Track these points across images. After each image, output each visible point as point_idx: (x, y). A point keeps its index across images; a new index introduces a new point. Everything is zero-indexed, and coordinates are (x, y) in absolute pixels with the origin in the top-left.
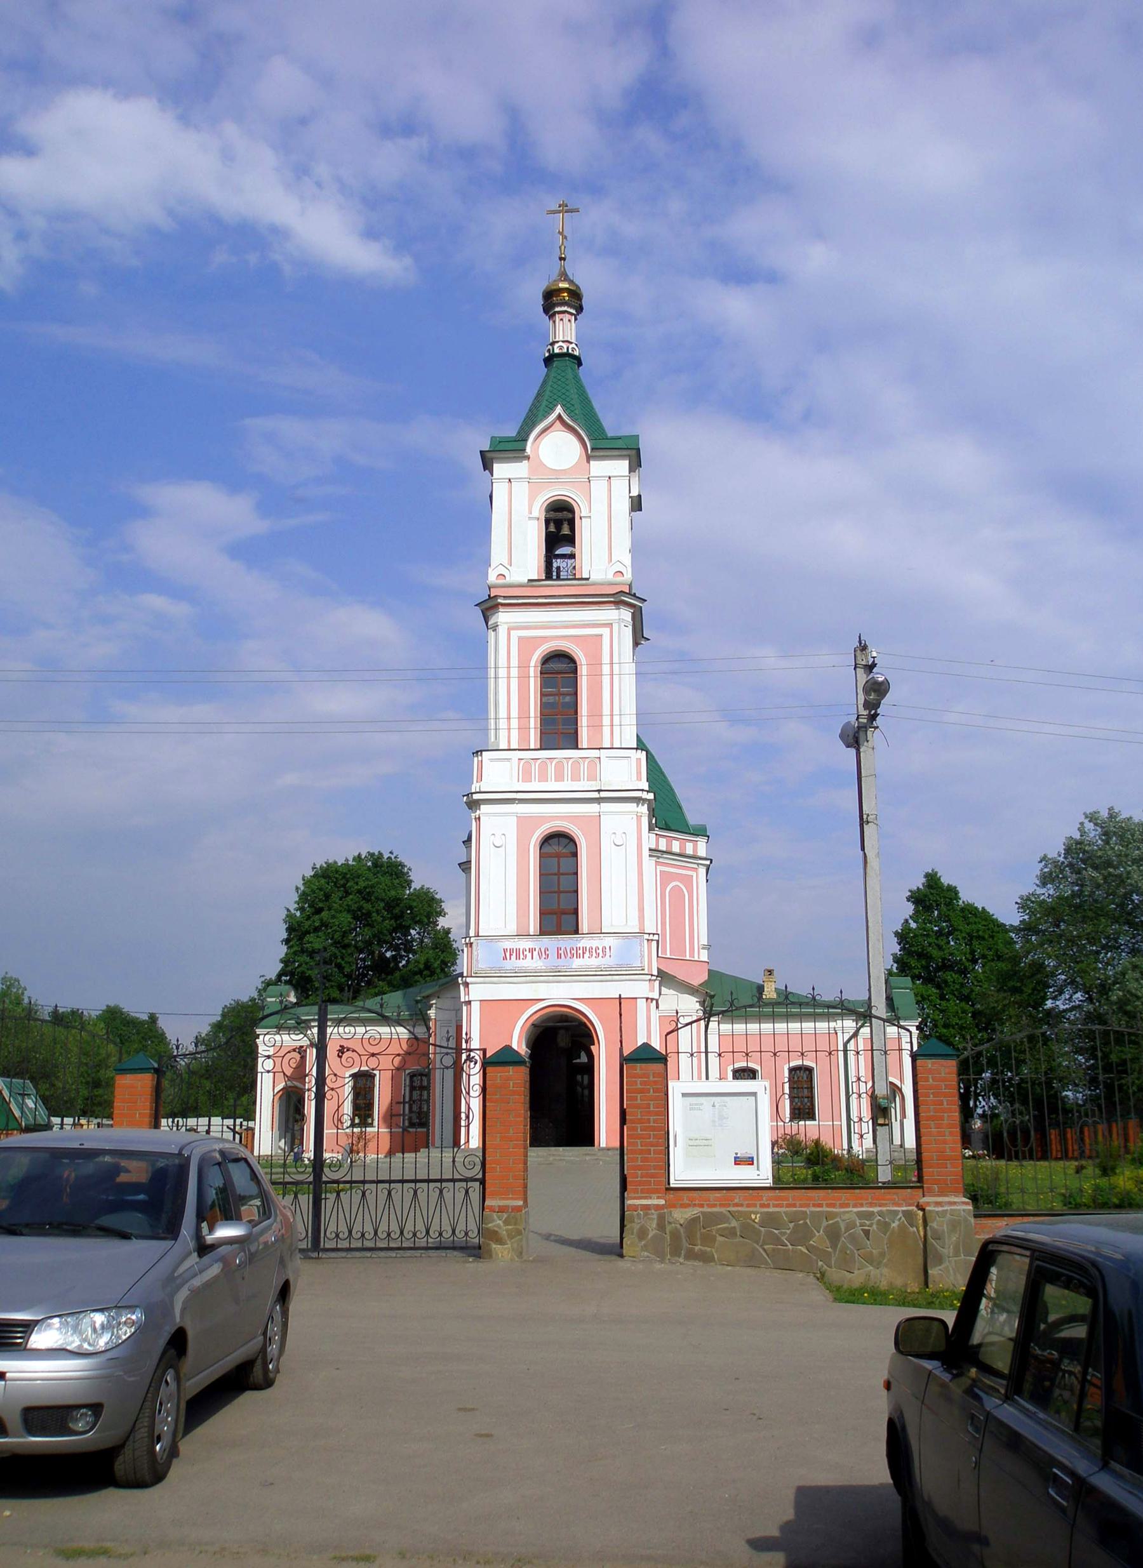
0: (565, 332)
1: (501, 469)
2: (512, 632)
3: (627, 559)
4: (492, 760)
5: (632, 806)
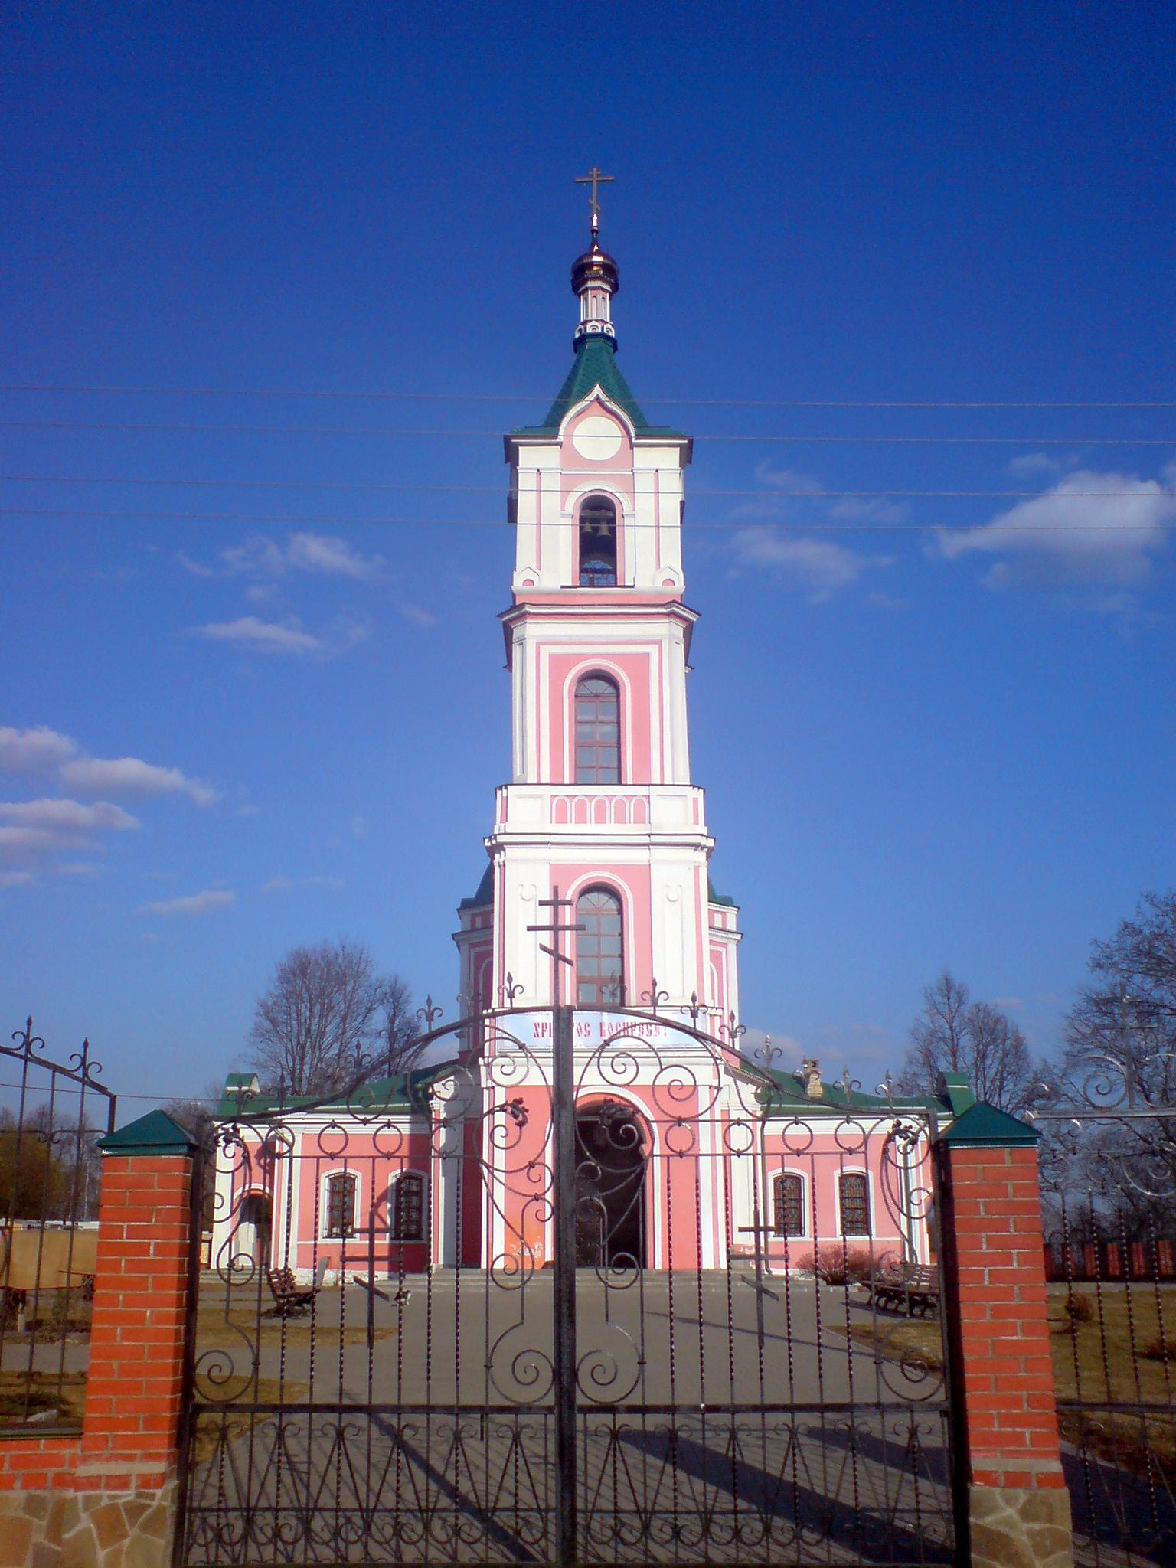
2: (542, 647)
3: (677, 565)
4: (519, 796)
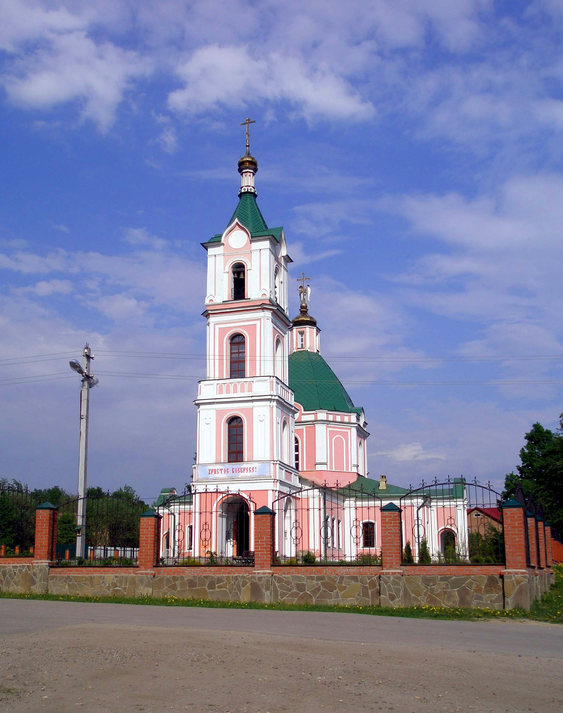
0: (248, 181)
1: (211, 251)
2: (216, 326)
4: (205, 385)
5: (268, 403)
